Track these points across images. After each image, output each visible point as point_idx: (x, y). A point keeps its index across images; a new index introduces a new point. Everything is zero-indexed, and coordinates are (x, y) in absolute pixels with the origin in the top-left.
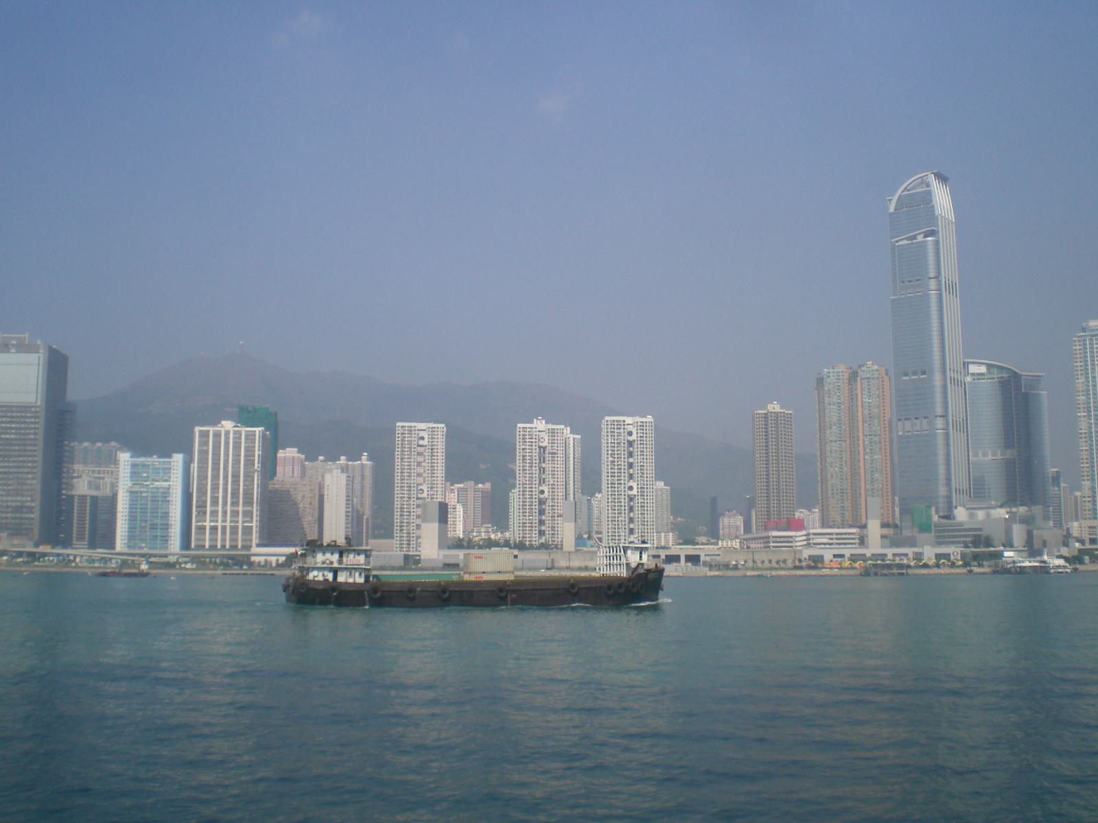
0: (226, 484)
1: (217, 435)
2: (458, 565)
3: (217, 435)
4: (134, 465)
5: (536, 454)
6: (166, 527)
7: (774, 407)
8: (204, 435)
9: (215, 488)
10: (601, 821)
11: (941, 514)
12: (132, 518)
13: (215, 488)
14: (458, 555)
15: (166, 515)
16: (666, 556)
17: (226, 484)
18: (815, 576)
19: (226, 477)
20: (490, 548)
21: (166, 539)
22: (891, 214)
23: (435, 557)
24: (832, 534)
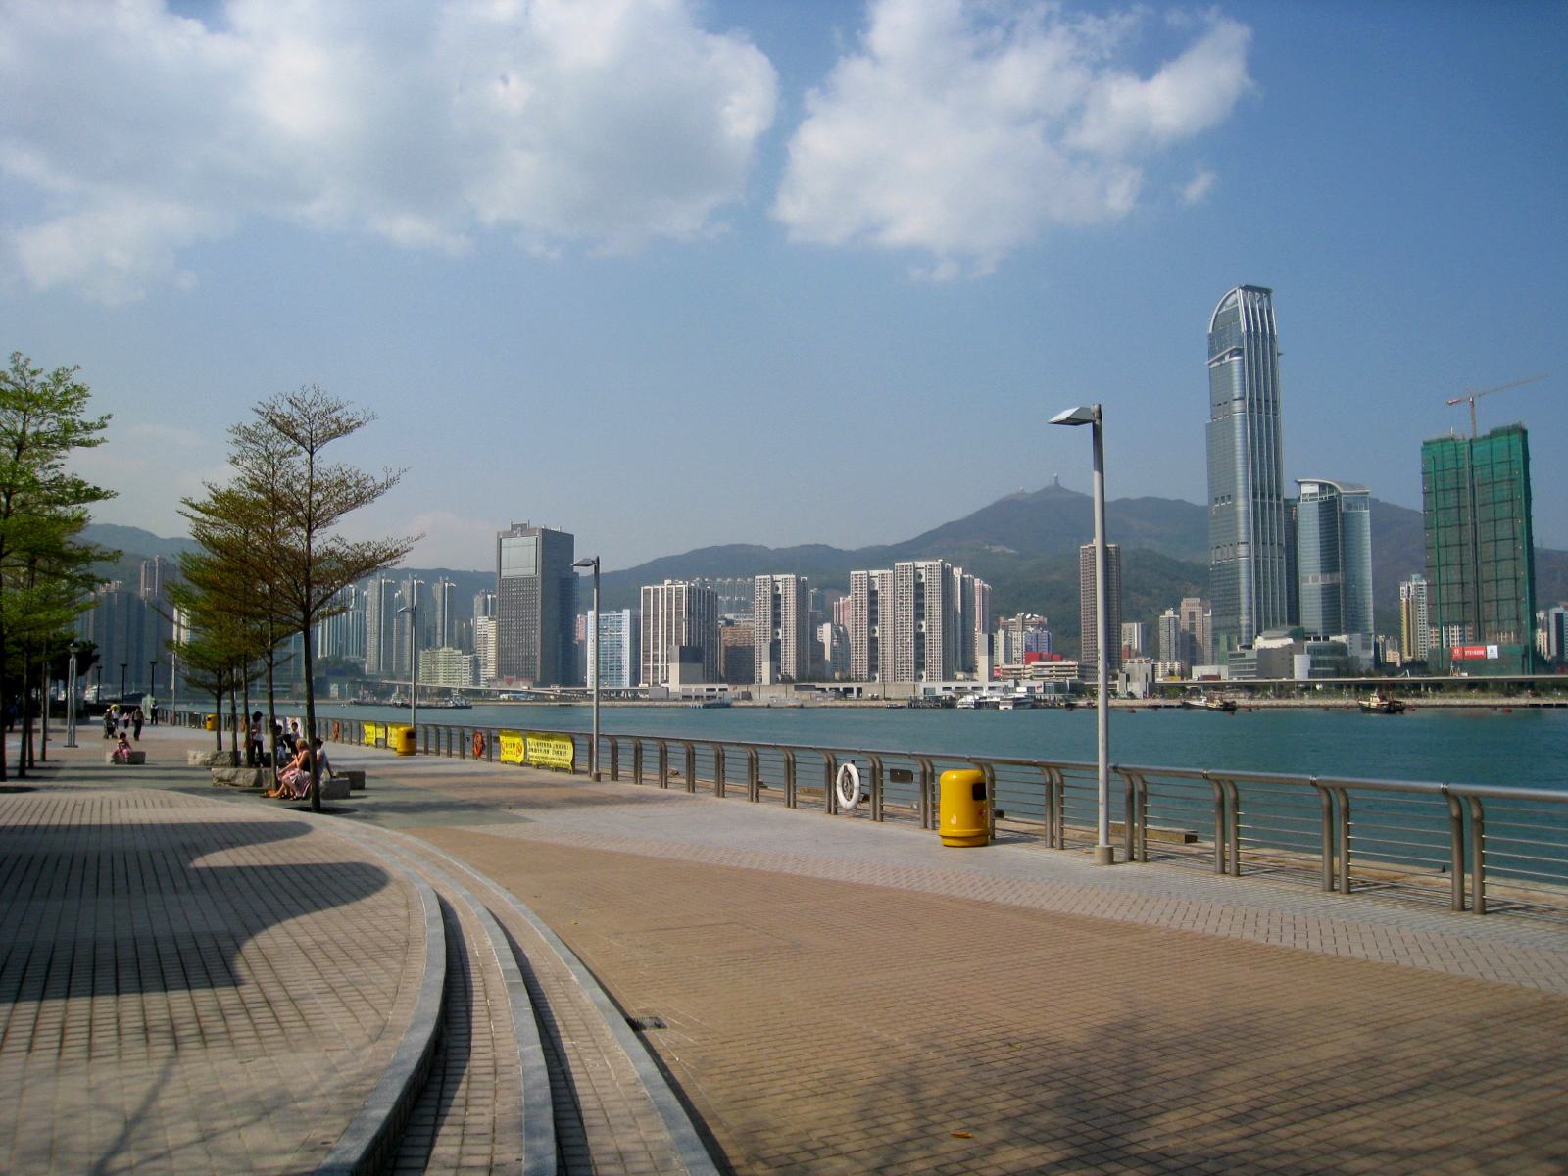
6: (620, 668)
11: (1243, 643)
15: (620, 659)
21: (620, 677)
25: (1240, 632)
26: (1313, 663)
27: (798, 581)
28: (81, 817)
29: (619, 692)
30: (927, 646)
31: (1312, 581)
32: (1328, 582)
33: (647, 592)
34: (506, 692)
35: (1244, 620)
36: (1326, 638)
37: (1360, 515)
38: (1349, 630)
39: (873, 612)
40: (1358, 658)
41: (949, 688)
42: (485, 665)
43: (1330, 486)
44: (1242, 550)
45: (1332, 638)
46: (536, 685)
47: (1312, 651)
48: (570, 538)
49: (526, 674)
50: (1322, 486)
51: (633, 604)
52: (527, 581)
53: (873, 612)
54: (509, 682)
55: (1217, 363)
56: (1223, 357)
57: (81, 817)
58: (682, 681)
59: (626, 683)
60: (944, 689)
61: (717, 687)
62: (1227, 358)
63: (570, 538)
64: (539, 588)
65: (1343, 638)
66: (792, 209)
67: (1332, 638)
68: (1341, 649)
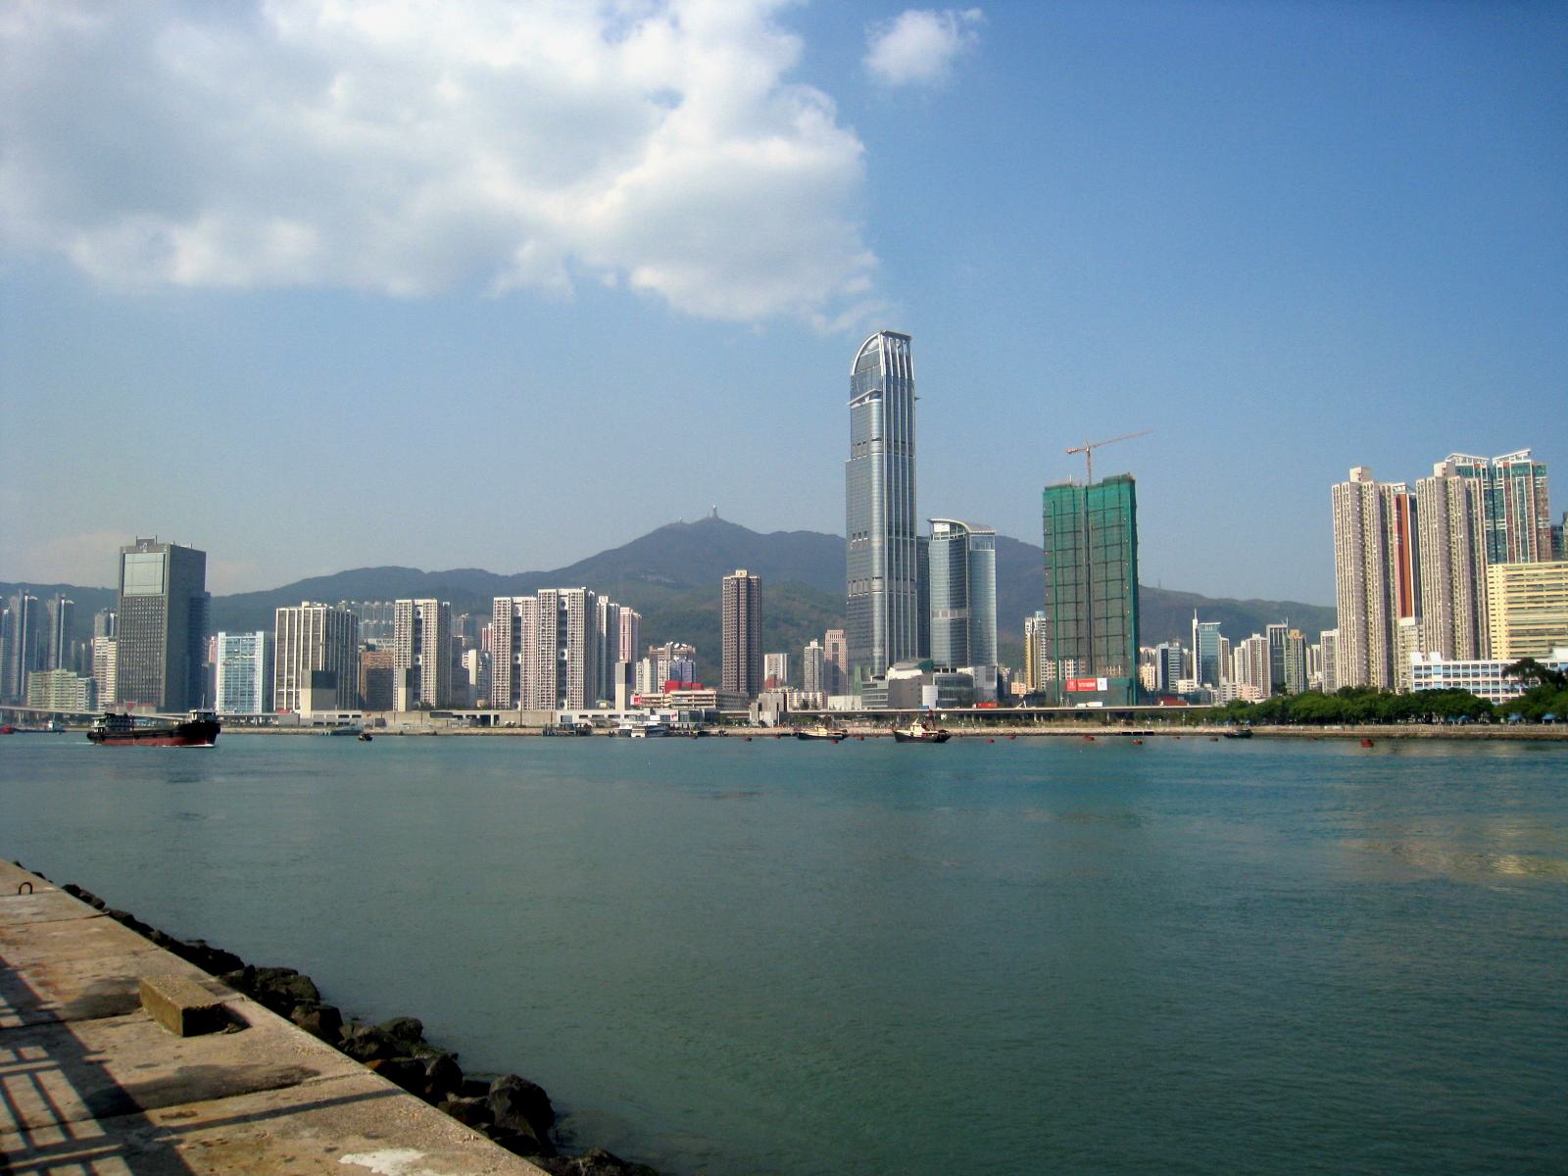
0: (298, 656)
1: (292, 614)
2: (322, 723)
3: (292, 614)
4: (228, 643)
5: (509, 625)
6: (252, 693)
7: (741, 574)
8: (282, 615)
9: (290, 660)
10: (1433, 1173)
11: (876, 675)
12: (227, 686)
13: (290, 660)
14: (864, 704)
15: (251, 684)
16: (481, 716)
17: (298, 656)
18: (1002, 735)
19: (298, 651)
20: (126, 716)
21: (252, 703)
22: (852, 377)
23: (308, 717)
24: (691, 696)
26: (941, 694)
27: (440, 605)
29: (250, 718)
31: (942, 615)
32: (956, 617)
33: (282, 615)
35: (877, 652)
37: (986, 554)
41: (586, 716)
43: (960, 526)
45: (959, 670)
46: (159, 710)
49: (148, 699)
50: (953, 526)
55: (857, 405)
56: (863, 399)
58: (313, 708)
61: (351, 713)
65: (969, 670)
67: (959, 670)
68: (966, 680)
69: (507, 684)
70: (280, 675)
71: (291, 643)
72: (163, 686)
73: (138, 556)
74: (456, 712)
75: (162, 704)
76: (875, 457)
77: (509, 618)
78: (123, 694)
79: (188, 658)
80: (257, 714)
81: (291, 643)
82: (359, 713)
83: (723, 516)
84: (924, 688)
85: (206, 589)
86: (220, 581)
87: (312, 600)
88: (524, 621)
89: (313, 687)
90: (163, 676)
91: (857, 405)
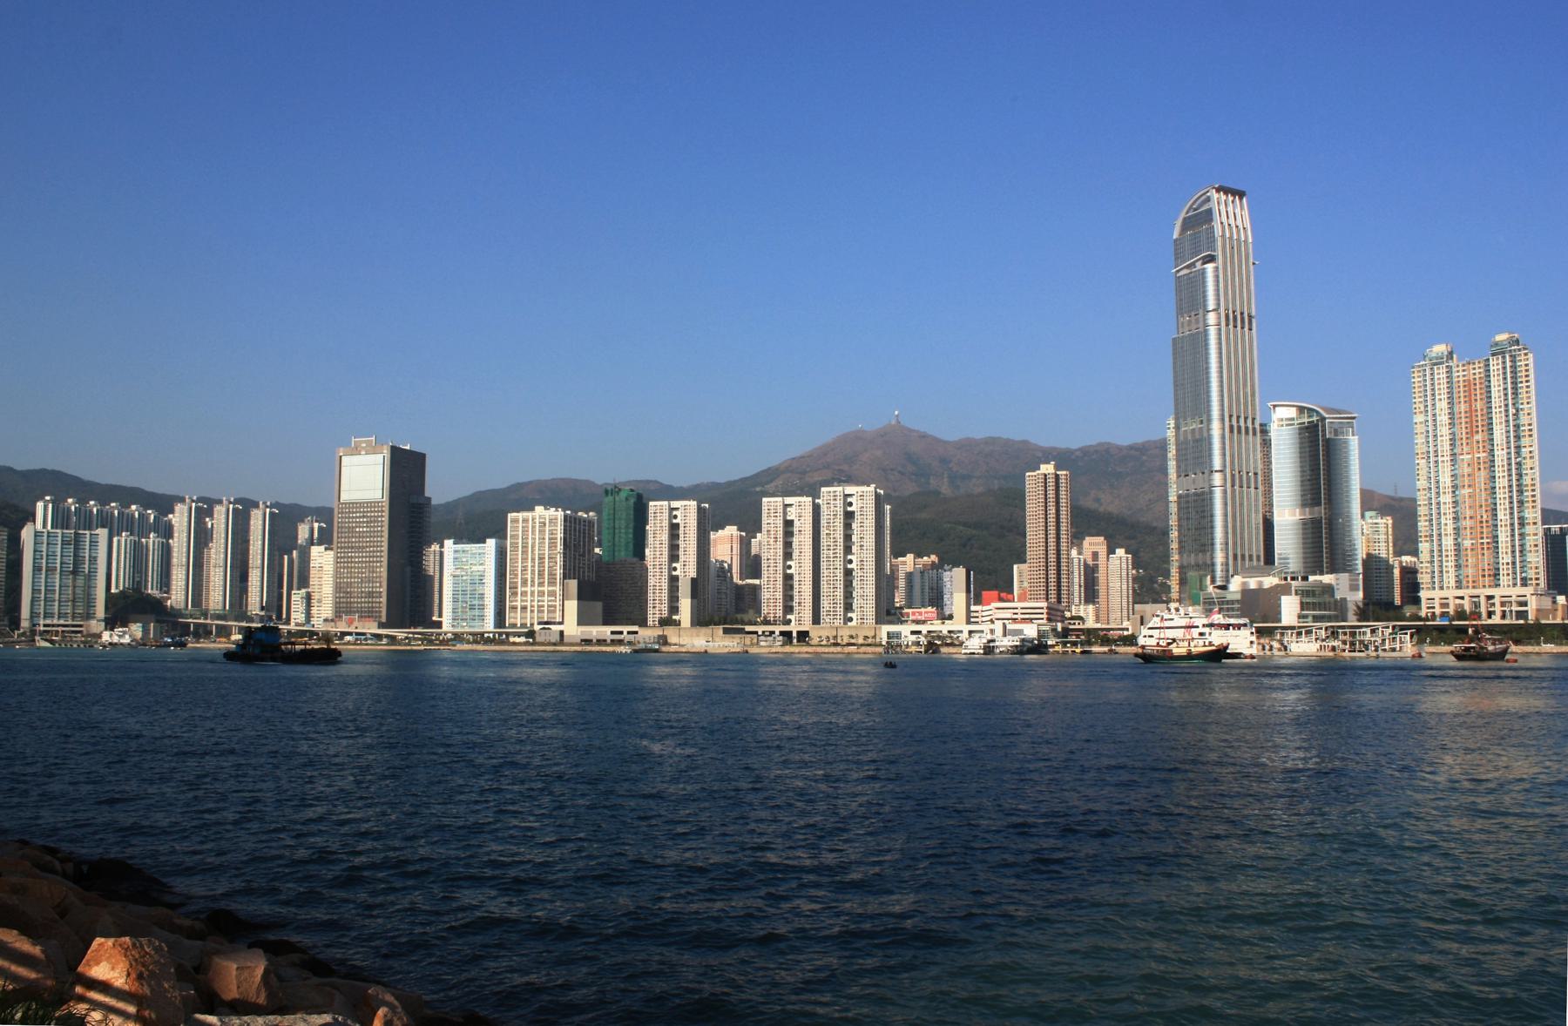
6: (482, 607)
11: (1219, 583)
15: (482, 597)
21: (482, 617)
25: (1213, 571)
26: (1303, 606)
27: (699, 508)
28: (816, 510)
29: (482, 634)
30: (796, 586)
31: (1288, 516)
32: (1308, 516)
33: (515, 521)
34: (350, 634)
35: (1219, 558)
36: (1305, 578)
37: (1346, 442)
38: (1333, 570)
39: (788, 545)
40: (1344, 600)
41: (919, 632)
42: (319, 601)
43: (1310, 410)
44: (1217, 479)
45: (1311, 578)
46: (381, 625)
47: (1303, 593)
48: (423, 456)
49: (368, 614)
50: (1301, 410)
51: (500, 533)
52: (371, 504)
53: (788, 545)
54: (350, 623)
55: (1186, 271)
56: (1193, 265)
57: (816, 510)
58: (580, 623)
59: (489, 625)
60: (913, 633)
61: (625, 629)
62: (1198, 265)
63: (423, 456)
64: (386, 514)
65: (1327, 579)
66: (217, 960)
67: (1311, 578)
68: (1329, 589)
69: (779, 595)
70: (514, 587)
71: (525, 552)
72: (384, 600)
73: (356, 459)
74: (748, 628)
75: (384, 620)
76: (1212, 332)
77: (780, 522)
78: (341, 610)
79: (408, 569)
80: (1284, 623)
81: (525, 552)
82: (635, 628)
83: (905, 422)
84: (1284, 598)
85: (427, 494)
86: (440, 488)
87: (547, 505)
88: (797, 523)
89: (580, 598)
90: (384, 590)
91: (1186, 271)
